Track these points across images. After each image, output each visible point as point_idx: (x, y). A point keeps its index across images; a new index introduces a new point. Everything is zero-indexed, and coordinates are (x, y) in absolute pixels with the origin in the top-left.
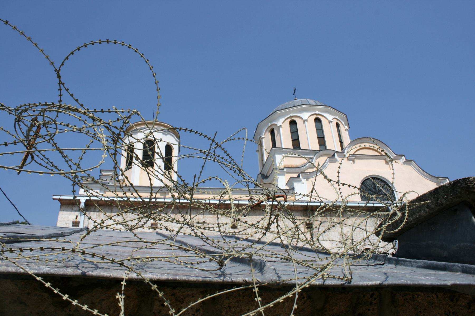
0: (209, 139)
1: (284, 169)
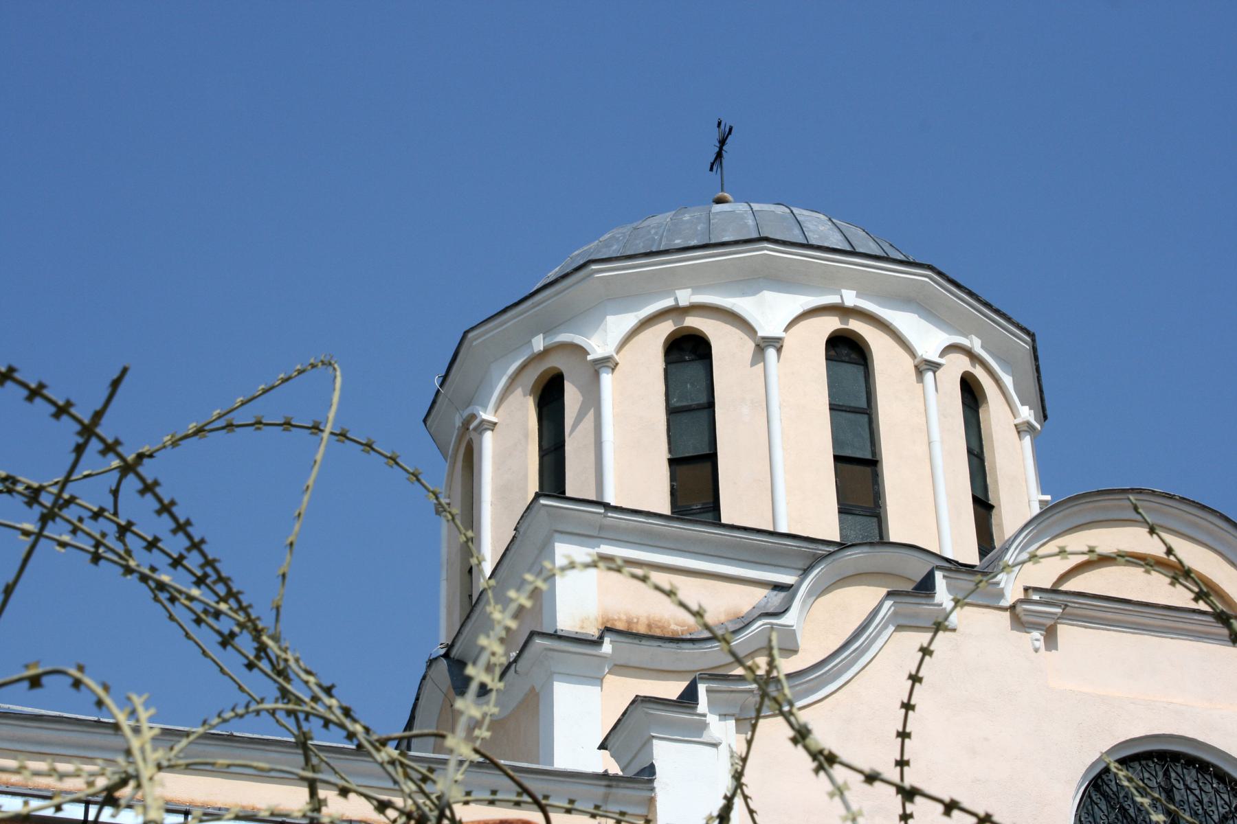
0: (62, 411)
1: (598, 642)
